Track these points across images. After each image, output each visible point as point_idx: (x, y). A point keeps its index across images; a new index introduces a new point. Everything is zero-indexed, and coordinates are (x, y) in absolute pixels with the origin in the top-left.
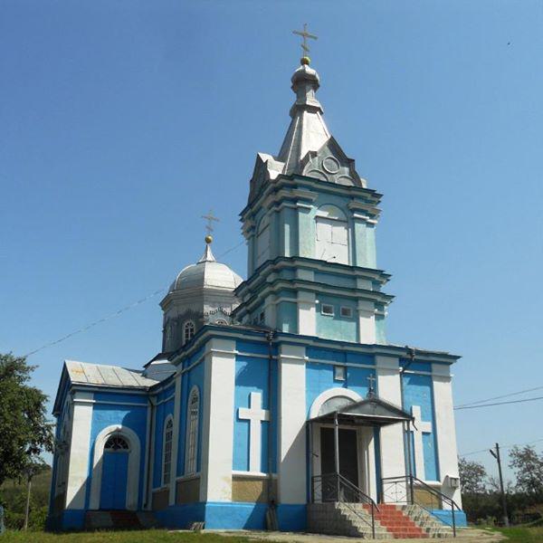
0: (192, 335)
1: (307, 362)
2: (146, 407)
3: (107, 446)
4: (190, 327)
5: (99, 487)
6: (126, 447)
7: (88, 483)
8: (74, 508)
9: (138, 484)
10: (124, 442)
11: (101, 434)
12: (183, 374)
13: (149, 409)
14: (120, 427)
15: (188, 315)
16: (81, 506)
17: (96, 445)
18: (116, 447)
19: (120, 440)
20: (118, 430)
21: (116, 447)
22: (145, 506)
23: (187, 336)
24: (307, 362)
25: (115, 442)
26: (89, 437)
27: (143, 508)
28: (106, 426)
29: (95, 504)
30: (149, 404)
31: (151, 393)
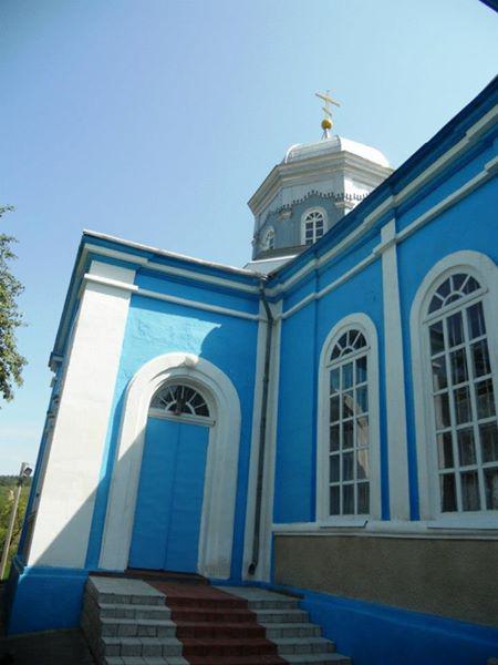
0: (319, 232)
1: (134, 295)
2: (257, 322)
3: (157, 401)
4: (315, 220)
5: (129, 524)
6: (204, 411)
7: (102, 497)
8: (55, 565)
9: (235, 458)
10: (199, 400)
11: (146, 367)
12: (399, 244)
13: (262, 328)
14: (195, 358)
15: (313, 199)
16: (76, 560)
17: (131, 395)
18: (180, 409)
19: (190, 392)
20: (189, 367)
21: (180, 409)
22: (252, 569)
23: (309, 234)
24: (134, 295)
25: (180, 396)
26: (114, 369)
27: (245, 574)
28: (159, 353)
29: (115, 555)
30: (262, 315)
31: (270, 292)
